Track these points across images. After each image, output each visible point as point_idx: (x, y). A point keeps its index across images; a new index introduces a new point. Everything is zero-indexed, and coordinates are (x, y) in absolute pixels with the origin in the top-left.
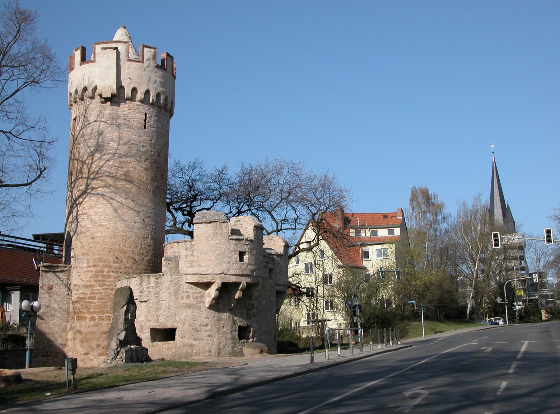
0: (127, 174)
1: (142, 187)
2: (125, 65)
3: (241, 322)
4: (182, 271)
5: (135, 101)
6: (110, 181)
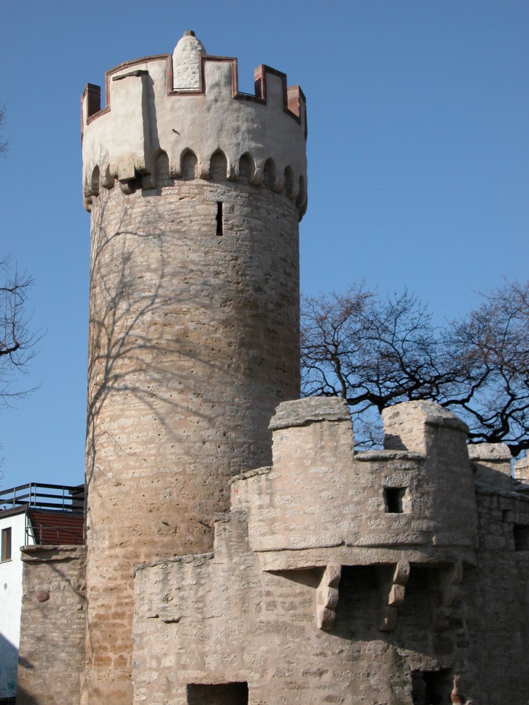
0: (181, 339)
1: (218, 363)
2: (164, 106)
3: (420, 660)
4: (255, 545)
5: (193, 178)
6: (147, 357)
